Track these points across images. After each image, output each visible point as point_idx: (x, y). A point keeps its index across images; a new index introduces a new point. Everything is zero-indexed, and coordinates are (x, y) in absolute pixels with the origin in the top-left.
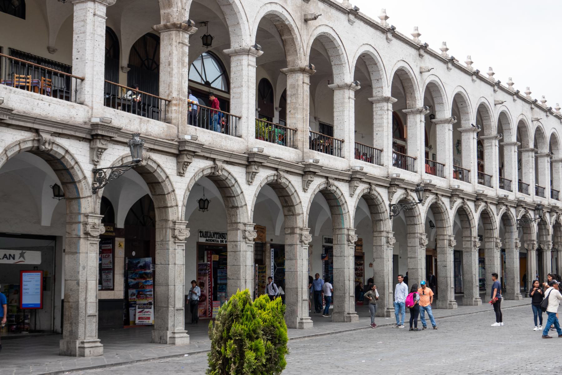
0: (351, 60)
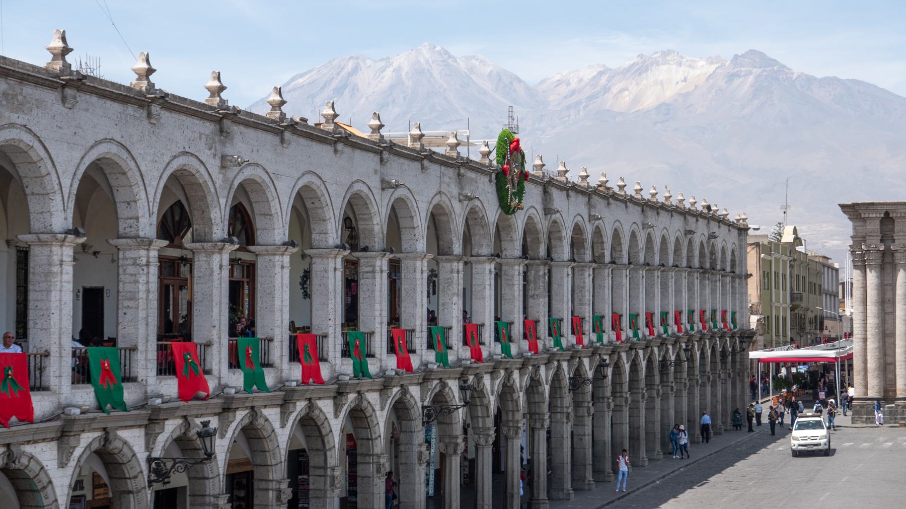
0: (66, 183)
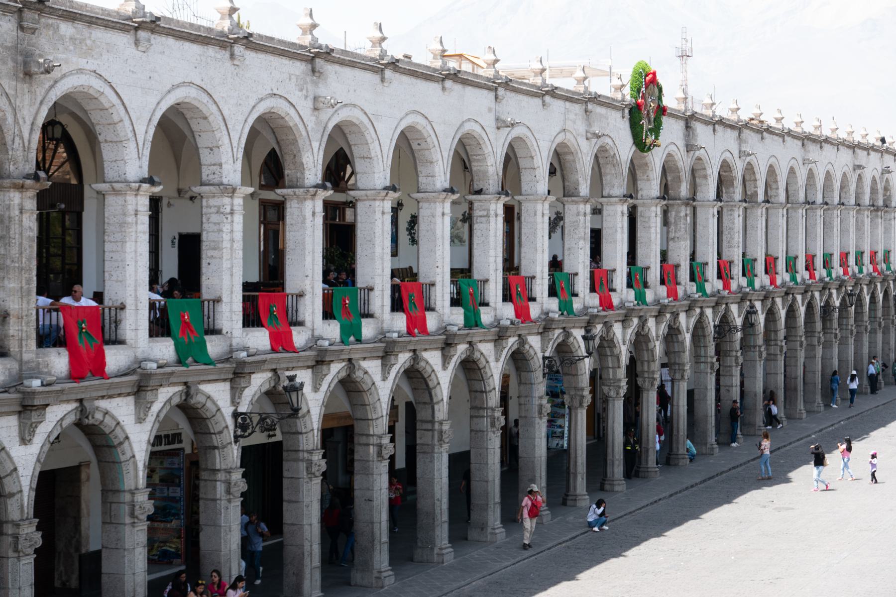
0: (140, 129)
